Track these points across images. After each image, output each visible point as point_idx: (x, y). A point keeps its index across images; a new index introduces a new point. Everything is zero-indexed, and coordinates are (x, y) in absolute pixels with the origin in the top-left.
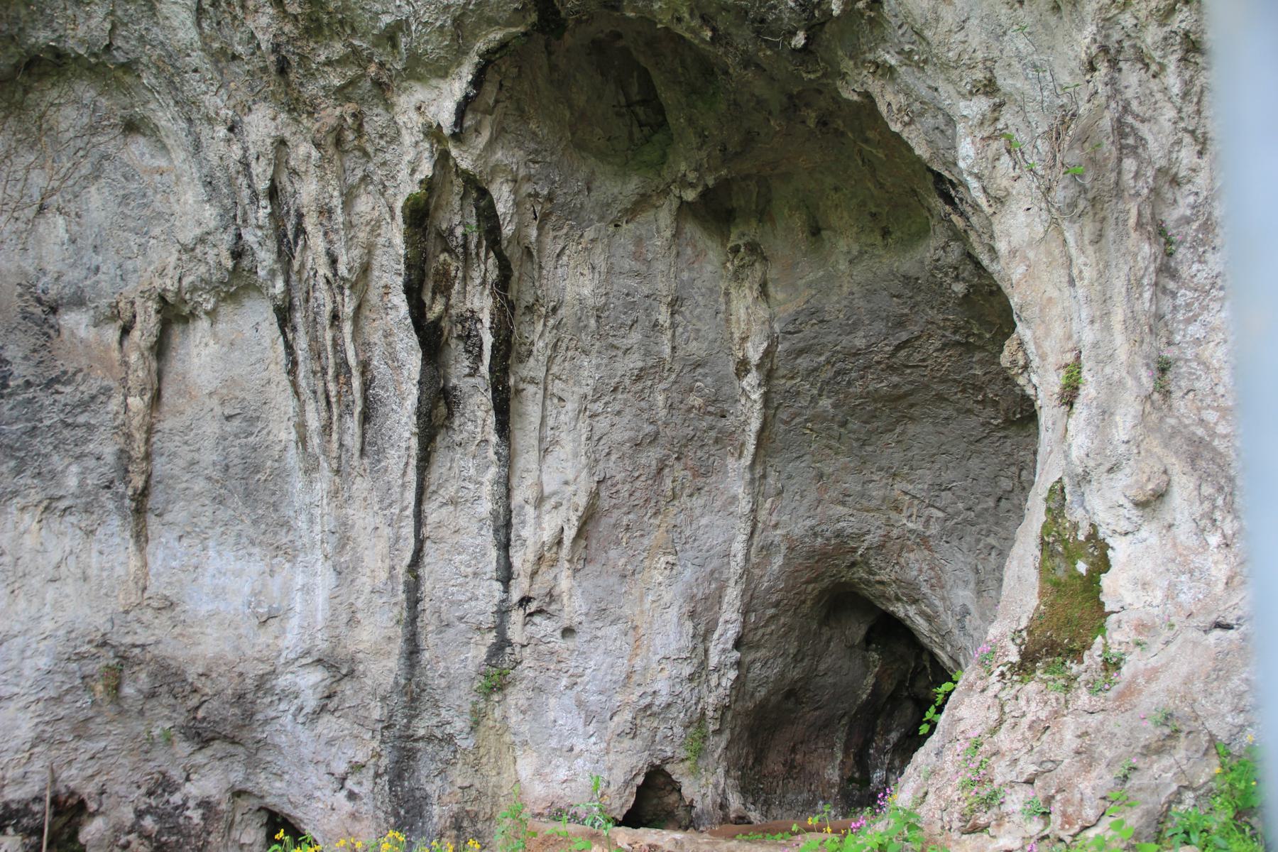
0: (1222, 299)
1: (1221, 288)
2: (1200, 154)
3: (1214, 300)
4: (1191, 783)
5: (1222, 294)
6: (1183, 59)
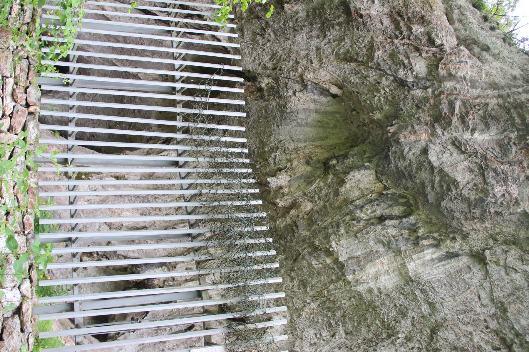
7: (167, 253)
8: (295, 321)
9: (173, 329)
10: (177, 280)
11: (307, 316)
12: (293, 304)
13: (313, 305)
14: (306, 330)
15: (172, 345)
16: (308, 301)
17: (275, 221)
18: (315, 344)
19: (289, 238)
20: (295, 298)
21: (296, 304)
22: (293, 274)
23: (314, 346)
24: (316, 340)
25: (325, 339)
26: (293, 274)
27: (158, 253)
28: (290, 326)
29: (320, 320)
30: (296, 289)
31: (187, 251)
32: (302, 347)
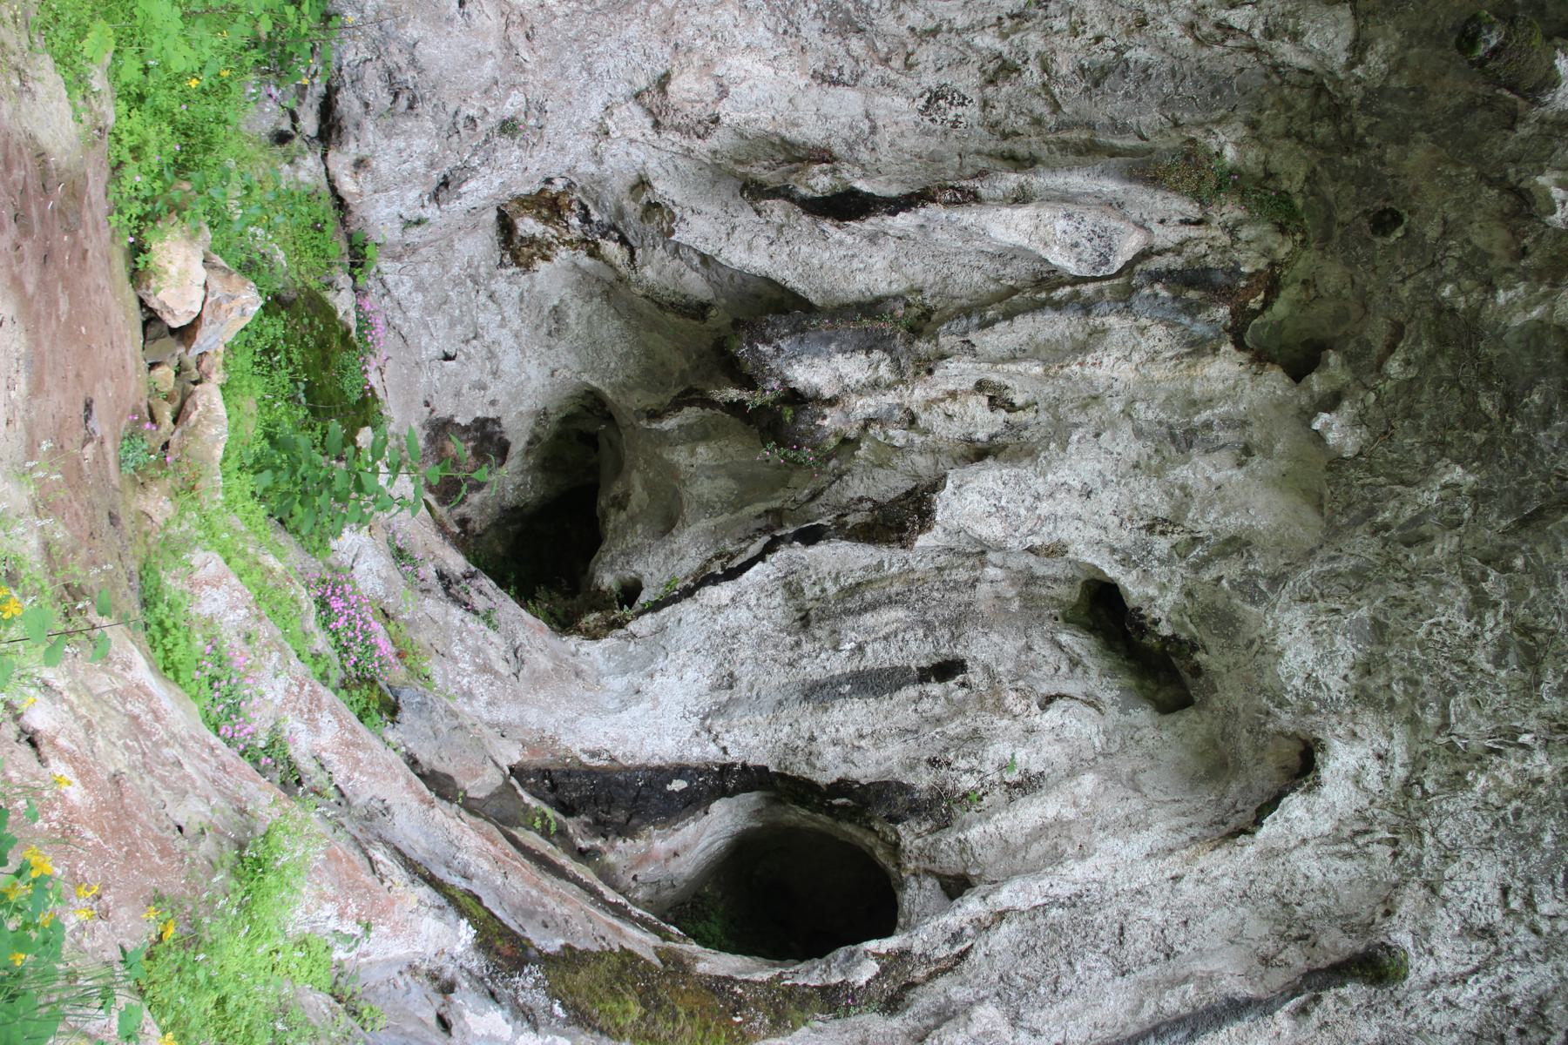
0: (776, 33)
1: (785, 32)
2: (912, 29)
3: (778, 23)
4: (169, 398)
5: (781, 31)
6: (1000, 56)
7: (904, 285)
8: (1425, 792)
9: (869, 649)
10: (926, 432)
11: (1493, 798)
12: (1446, 716)
13: (1542, 764)
14: (1467, 857)
15: (852, 729)
16: (1525, 738)
17: (1490, 287)
18: (1487, 932)
19: (1536, 398)
20: (1463, 697)
21: (1460, 729)
22: (1493, 583)
23: (1483, 945)
24: (1498, 914)
25: (1545, 927)
26: (1493, 583)
27: (860, 277)
28: (1395, 806)
29: (1548, 838)
30: (1481, 658)
31: (999, 298)
32: (1427, 930)
